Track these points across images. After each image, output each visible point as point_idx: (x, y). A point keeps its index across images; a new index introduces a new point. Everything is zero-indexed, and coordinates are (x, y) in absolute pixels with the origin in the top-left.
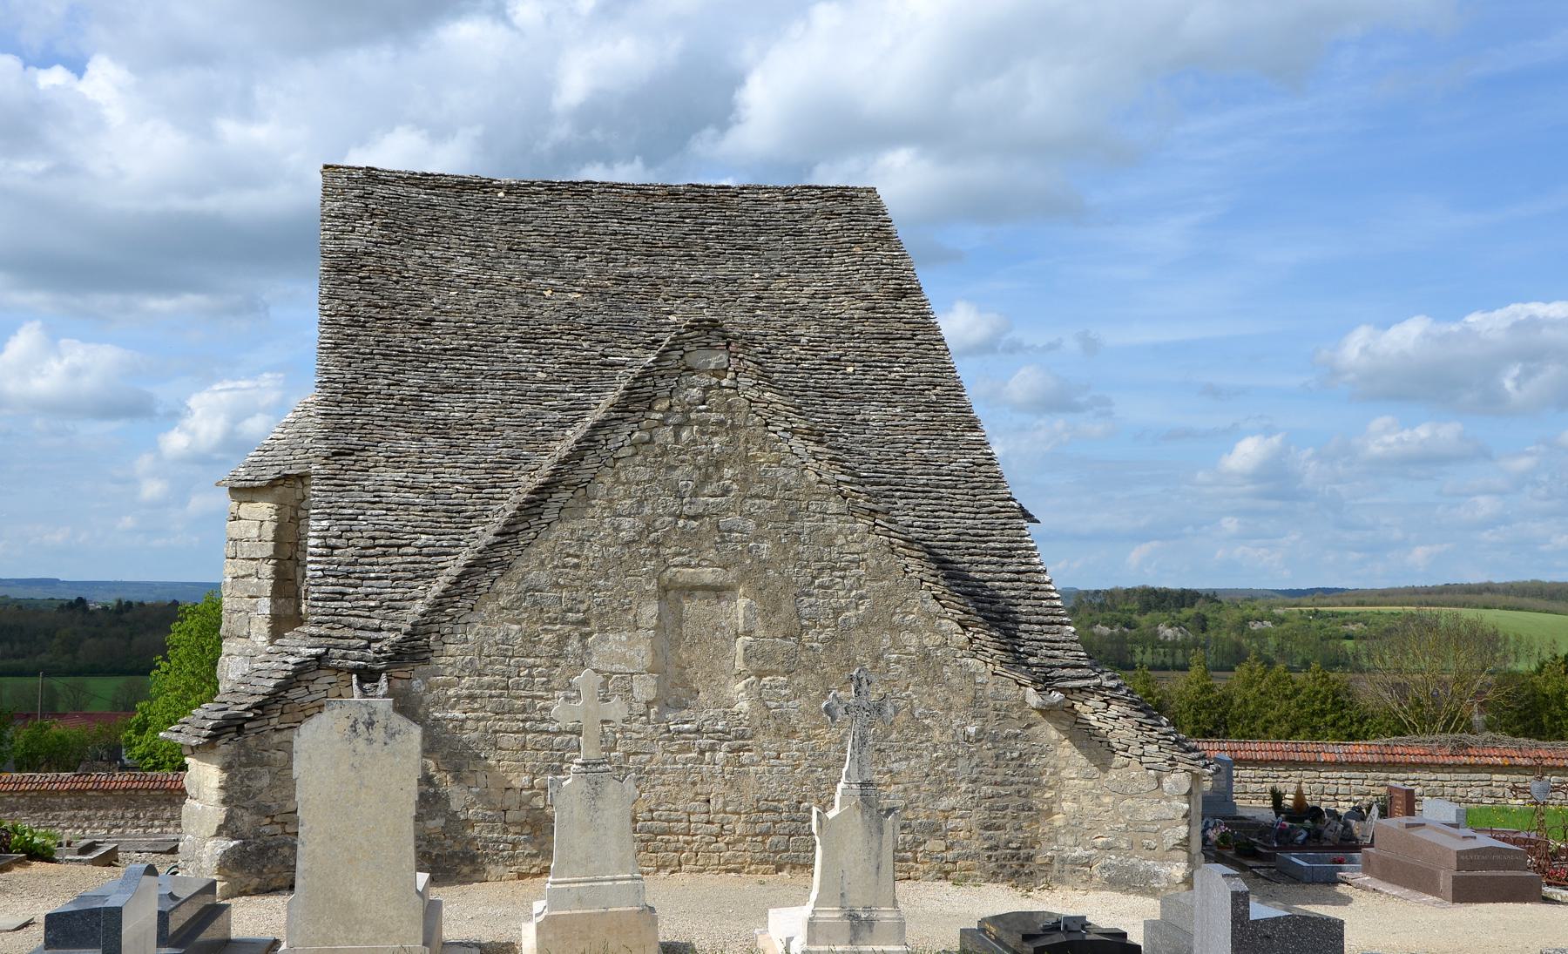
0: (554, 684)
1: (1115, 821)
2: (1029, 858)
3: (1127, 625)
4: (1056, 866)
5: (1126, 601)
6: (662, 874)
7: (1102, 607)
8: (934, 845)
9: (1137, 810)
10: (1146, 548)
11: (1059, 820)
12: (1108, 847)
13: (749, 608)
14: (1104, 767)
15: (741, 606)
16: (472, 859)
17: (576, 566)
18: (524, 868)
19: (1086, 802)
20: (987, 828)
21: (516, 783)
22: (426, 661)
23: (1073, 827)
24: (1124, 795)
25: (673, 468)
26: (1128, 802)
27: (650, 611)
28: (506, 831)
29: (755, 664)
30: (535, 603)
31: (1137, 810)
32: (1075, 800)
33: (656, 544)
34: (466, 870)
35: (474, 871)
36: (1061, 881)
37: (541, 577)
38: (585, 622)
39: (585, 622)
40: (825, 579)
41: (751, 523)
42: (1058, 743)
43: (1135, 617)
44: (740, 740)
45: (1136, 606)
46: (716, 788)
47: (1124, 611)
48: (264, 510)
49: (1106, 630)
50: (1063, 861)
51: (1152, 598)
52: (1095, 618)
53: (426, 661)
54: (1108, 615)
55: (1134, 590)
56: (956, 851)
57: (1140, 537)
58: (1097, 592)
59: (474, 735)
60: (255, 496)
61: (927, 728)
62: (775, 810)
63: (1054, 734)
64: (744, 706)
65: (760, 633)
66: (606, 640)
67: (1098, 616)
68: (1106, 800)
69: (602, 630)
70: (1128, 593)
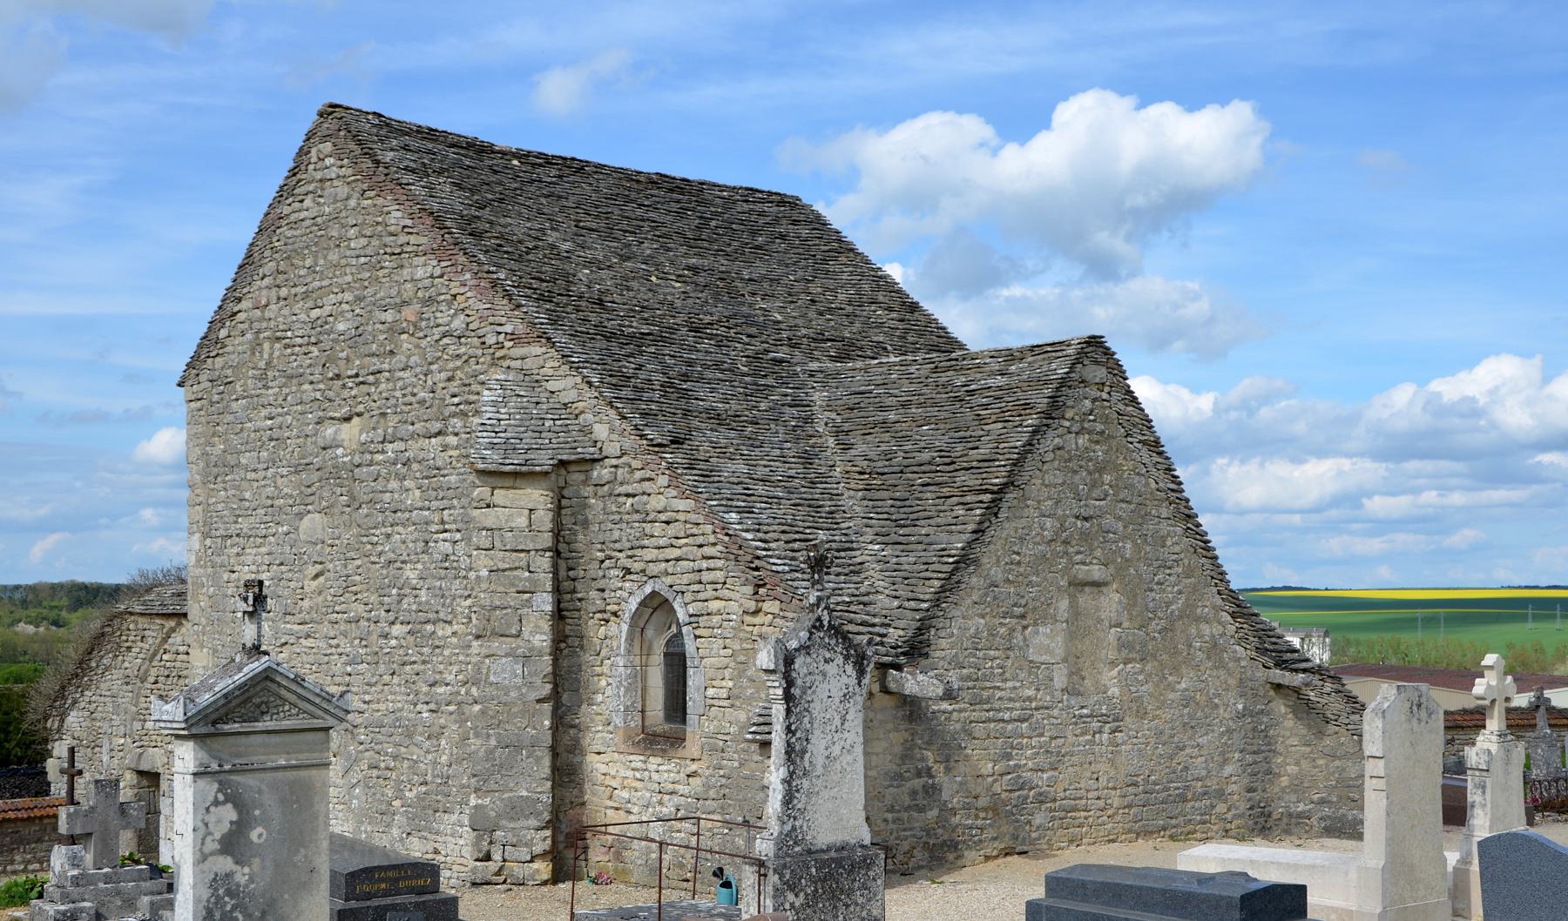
0: (1007, 675)
1: (1328, 780)
2: (1269, 815)
3: (56, 623)
4: (1285, 820)
5: (52, 598)
6: (1073, 847)
7: (24, 603)
8: (1221, 808)
9: (1344, 769)
10: (53, 539)
11: (1285, 781)
12: (1322, 802)
13: (1120, 602)
14: (1321, 734)
15: (1111, 602)
16: (953, 846)
17: (1019, 563)
18: (989, 851)
19: (1305, 764)
20: (1249, 791)
21: (984, 772)
22: (926, 655)
23: (1297, 787)
24: (1334, 757)
25: (1075, 472)
26: (1337, 763)
27: (1064, 604)
28: (977, 817)
29: (1125, 652)
30: (995, 598)
31: (1344, 769)
32: (1297, 763)
33: (1066, 542)
34: (951, 857)
35: (957, 858)
36: (1288, 832)
37: (997, 573)
38: (1023, 616)
39: (1023, 616)
40: (1160, 577)
41: (1120, 525)
42: (1284, 716)
43: (64, 613)
44: (1114, 721)
45: (65, 602)
46: (1103, 767)
47: (52, 608)
48: (537, 497)
49: (31, 629)
50: (1290, 815)
51: (82, 594)
52: (17, 615)
53: (926, 655)
54: (33, 612)
55: (61, 586)
56: (1233, 812)
57: (43, 527)
58: (17, 587)
59: (958, 726)
60: (518, 482)
61: (1217, 706)
62: (1135, 784)
63: (1283, 709)
64: (1114, 691)
65: (1126, 624)
66: (1037, 633)
67: (20, 613)
68: (1321, 762)
69: (1035, 624)
70: (54, 589)
